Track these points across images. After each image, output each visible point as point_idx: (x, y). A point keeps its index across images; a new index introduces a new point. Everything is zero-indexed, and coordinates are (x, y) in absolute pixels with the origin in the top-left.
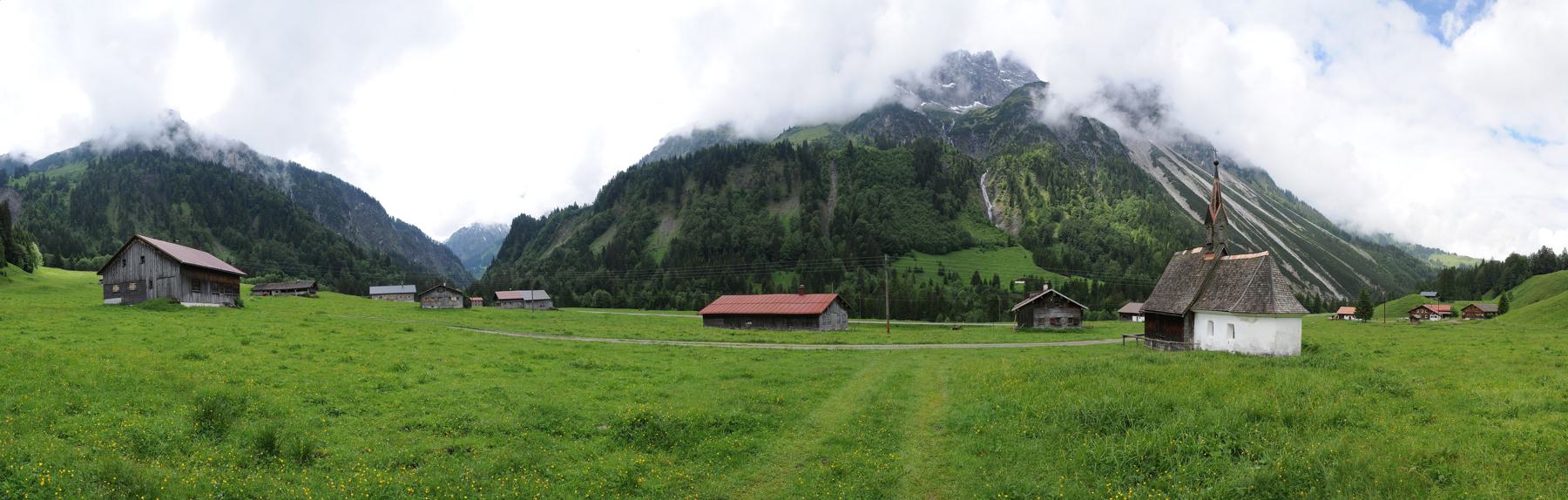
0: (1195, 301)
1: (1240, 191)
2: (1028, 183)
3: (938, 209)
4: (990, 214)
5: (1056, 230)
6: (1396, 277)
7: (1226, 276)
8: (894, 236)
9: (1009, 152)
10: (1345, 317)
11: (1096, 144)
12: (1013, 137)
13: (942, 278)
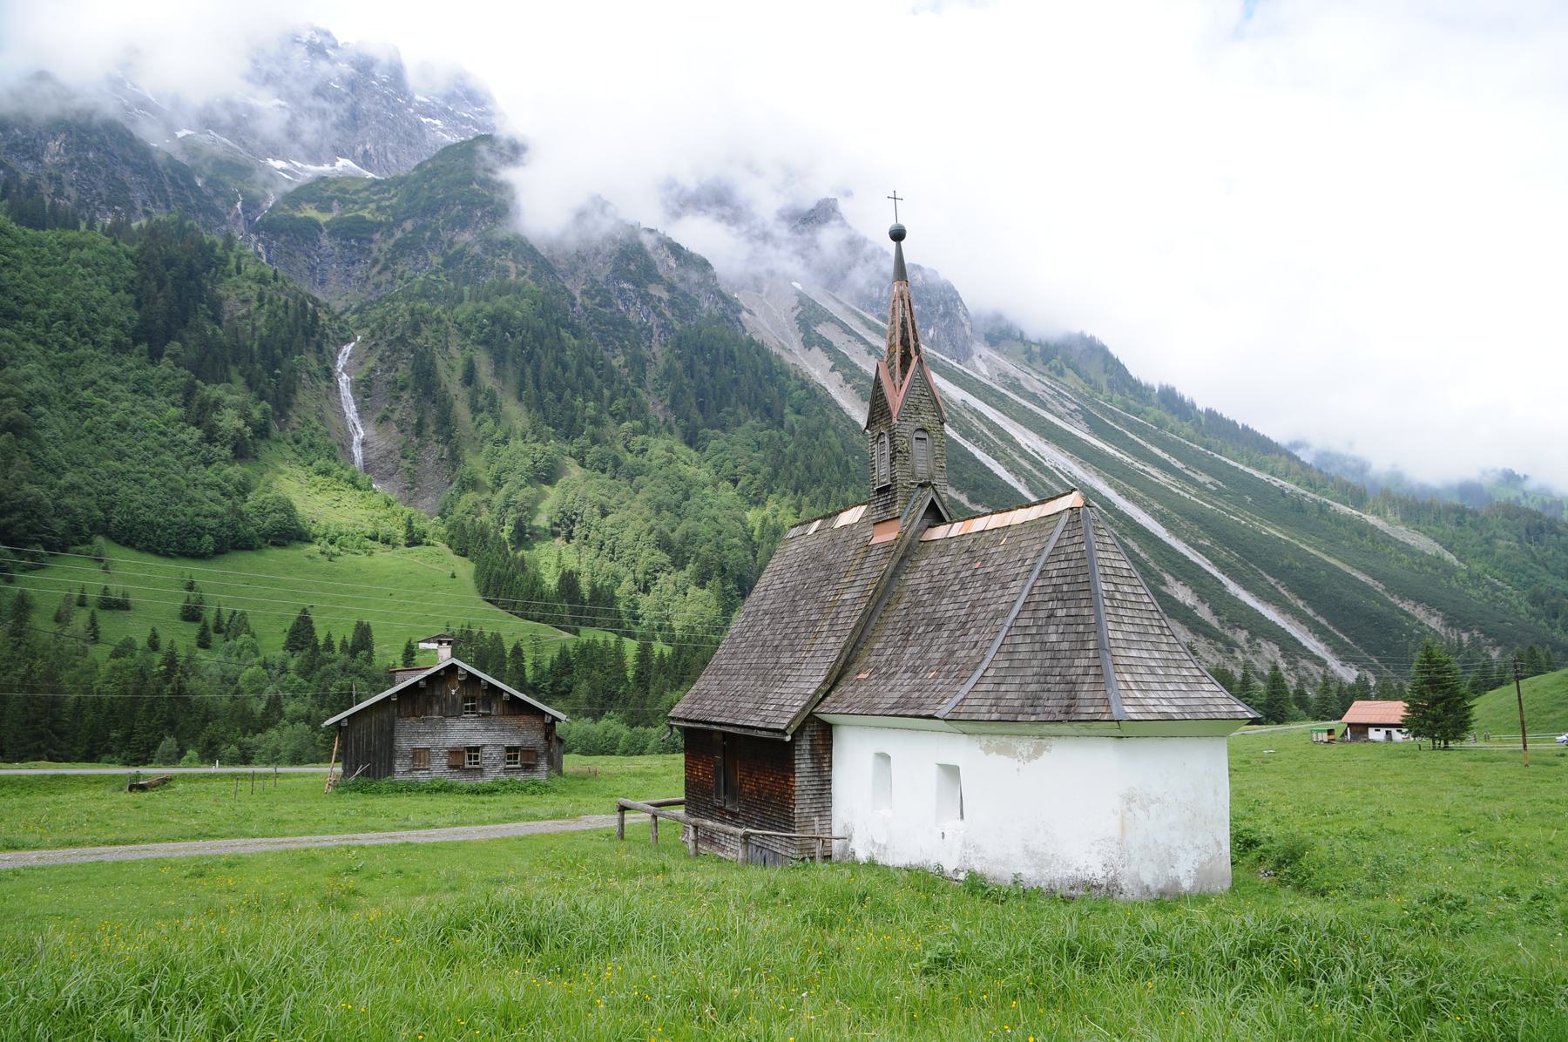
0: (833, 682)
1: (1033, 397)
2: (470, 378)
3: (197, 424)
4: (358, 452)
5: (545, 506)
6: (1536, 600)
7: (937, 592)
8: (35, 489)
9: (424, 295)
10: (1373, 734)
11: (656, 291)
12: (436, 260)
13: (194, 629)
